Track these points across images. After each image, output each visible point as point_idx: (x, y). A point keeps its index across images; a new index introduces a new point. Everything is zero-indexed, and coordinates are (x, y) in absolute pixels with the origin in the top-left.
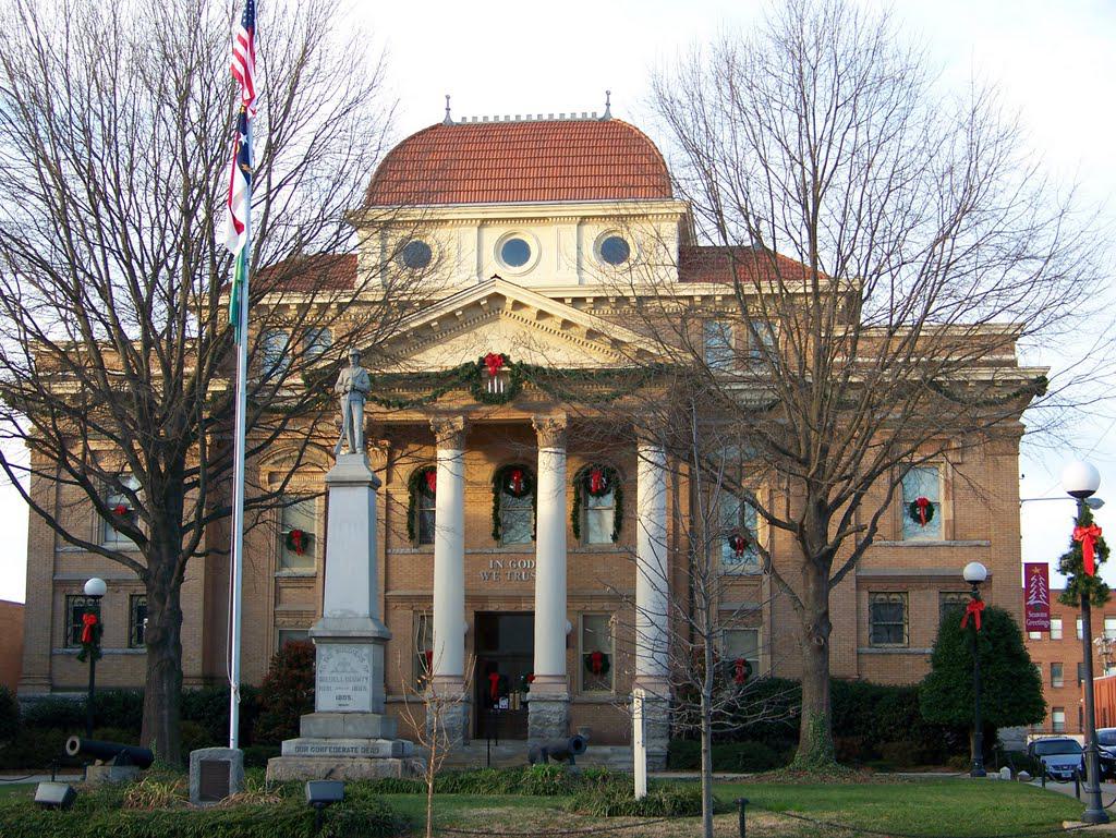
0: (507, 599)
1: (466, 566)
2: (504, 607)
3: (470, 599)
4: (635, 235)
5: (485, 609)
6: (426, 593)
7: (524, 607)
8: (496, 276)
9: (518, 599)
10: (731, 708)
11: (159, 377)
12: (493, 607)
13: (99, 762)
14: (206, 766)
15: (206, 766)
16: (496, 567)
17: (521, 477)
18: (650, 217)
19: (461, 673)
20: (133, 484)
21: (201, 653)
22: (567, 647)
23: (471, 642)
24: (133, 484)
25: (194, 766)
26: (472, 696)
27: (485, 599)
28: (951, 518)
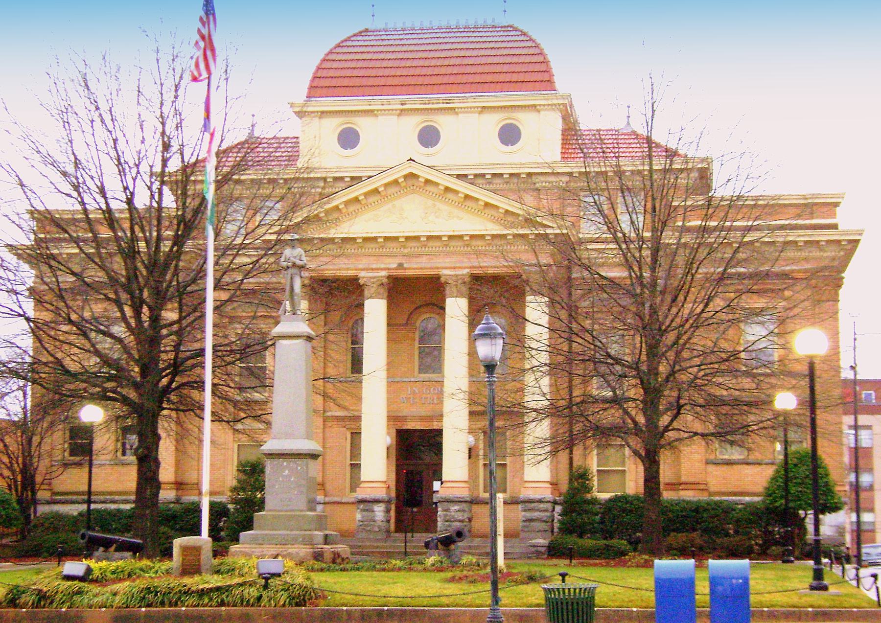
0: (422, 419)
1: (388, 392)
2: (418, 426)
3: (392, 418)
4: (525, 121)
5: (405, 427)
6: (356, 414)
7: (435, 426)
8: (411, 159)
9: (430, 418)
10: (162, 282)
11: (144, 252)
12: (411, 425)
13: (101, 549)
14: (185, 549)
15: (185, 549)
16: (414, 393)
17: (408, 369)
18: (538, 107)
19: (384, 479)
20: (119, 330)
21: (161, 468)
22: (470, 457)
23: (393, 453)
24: (119, 330)
25: (176, 551)
26: (393, 494)
27: (404, 419)
28: (165, 427)
